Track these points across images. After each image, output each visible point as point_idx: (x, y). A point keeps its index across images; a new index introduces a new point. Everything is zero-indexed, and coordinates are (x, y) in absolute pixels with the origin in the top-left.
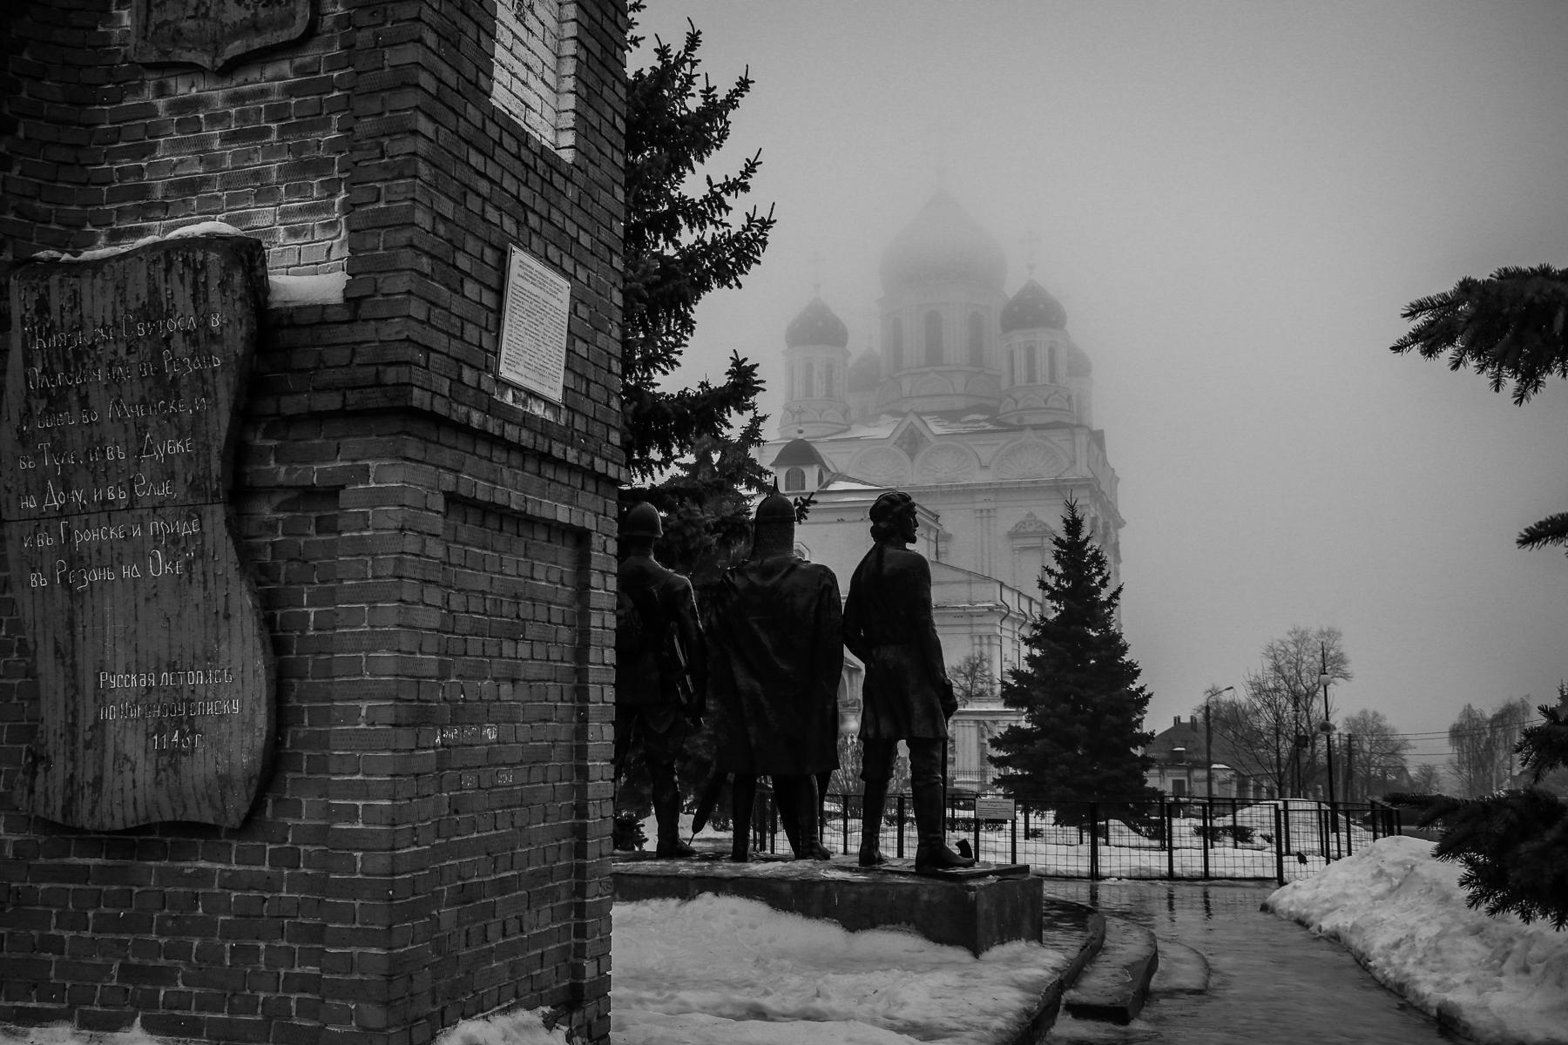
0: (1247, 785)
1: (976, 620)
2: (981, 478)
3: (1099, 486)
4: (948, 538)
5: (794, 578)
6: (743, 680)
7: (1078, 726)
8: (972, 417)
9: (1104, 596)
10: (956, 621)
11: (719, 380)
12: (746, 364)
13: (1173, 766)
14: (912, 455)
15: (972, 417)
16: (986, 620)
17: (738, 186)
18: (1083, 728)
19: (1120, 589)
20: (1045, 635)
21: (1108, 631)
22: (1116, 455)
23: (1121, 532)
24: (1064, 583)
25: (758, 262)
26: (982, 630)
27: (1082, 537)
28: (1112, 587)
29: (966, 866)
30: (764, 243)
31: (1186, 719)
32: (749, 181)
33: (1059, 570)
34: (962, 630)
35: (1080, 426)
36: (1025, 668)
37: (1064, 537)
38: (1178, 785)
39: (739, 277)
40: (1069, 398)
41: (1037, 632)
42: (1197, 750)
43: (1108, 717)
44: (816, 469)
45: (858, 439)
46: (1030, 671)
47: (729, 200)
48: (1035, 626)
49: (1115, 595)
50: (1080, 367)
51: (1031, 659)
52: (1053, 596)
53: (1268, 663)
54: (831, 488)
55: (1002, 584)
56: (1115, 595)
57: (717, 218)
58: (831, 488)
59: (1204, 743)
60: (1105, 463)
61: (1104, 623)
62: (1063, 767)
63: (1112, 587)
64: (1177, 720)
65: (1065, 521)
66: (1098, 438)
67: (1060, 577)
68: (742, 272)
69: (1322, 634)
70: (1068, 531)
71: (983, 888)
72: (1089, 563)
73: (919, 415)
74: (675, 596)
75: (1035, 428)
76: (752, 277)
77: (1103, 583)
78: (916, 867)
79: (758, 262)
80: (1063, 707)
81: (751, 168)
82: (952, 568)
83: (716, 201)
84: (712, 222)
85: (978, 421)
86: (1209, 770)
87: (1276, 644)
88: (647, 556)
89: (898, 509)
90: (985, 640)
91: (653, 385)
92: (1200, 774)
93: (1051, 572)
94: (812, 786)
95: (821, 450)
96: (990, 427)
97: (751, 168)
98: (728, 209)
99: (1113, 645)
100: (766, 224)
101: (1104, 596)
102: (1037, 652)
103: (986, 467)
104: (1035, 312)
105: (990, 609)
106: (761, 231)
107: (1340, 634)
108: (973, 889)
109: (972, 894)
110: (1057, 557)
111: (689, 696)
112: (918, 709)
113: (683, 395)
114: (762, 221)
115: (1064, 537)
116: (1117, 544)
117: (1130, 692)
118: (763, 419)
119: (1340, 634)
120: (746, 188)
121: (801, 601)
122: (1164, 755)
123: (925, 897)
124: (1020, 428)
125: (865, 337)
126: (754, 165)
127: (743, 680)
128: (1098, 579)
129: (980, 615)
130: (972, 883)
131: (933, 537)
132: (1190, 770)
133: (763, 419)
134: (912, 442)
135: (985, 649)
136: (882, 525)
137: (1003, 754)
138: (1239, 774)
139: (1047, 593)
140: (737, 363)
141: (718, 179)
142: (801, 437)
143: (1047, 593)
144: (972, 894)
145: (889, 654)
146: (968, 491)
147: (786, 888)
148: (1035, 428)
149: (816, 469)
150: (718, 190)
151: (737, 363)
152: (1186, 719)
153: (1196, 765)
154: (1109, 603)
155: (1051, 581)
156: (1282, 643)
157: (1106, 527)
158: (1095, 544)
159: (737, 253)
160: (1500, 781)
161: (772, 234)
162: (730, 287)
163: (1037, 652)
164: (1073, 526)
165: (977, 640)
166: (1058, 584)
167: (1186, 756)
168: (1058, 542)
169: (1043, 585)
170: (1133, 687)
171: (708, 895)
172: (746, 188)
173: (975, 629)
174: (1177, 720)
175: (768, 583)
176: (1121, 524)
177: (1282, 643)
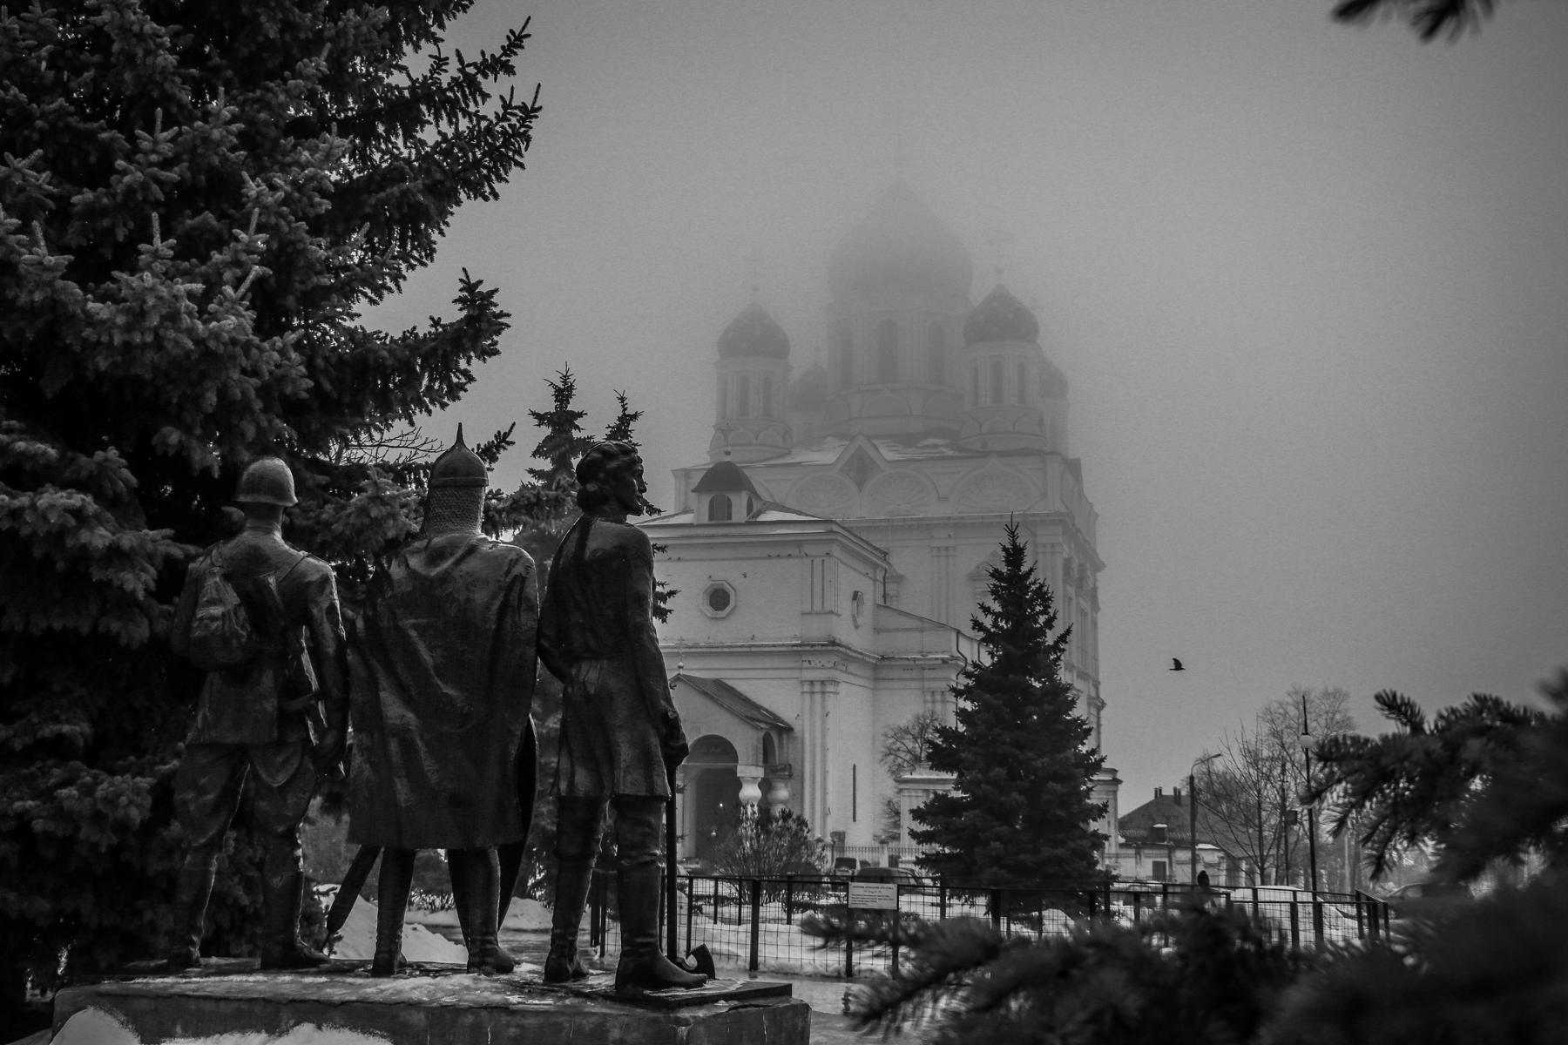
0: (1238, 869)
1: (928, 674)
2: (937, 511)
3: (1074, 525)
4: (899, 579)
5: (472, 564)
6: (394, 710)
7: (1015, 795)
8: (931, 441)
9: (1050, 638)
10: (907, 675)
11: (453, 314)
12: (483, 289)
13: (1153, 846)
14: (860, 484)
15: (931, 441)
16: (939, 674)
17: (498, 65)
18: (1021, 798)
19: (1068, 631)
20: (981, 684)
21: (1051, 679)
22: (1095, 488)
23: (1099, 575)
24: (1003, 624)
25: (522, 166)
26: (934, 685)
27: (1024, 569)
28: (1059, 628)
29: (688, 986)
30: (528, 139)
31: (1168, 791)
32: (513, 61)
33: (997, 607)
34: (914, 684)
35: (1051, 453)
36: (952, 722)
37: (1004, 569)
38: (1159, 869)
39: (496, 185)
40: (1041, 423)
41: (971, 682)
42: (1181, 827)
43: (1051, 784)
44: (744, 497)
45: (799, 464)
46: (962, 728)
47: (487, 84)
48: (969, 675)
49: (1063, 638)
50: (1055, 385)
51: (962, 715)
52: (989, 638)
53: (1265, 728)
54: (762, 518)
55: (958, 632)
56: (1063, 638)
57: (472, 109)
58: (762, 518)
59: (1188, 817)
60: (1081, 495)
61: (1049, 671)
62: (997, 844)
63: (1059, 628)
64: (1158, 792)
65: (1005, 549)
66: (1073, 468)
67: (997, 615)
68: (500, 179)
69: (1326, 695)
70: (1008, 562)
71: (703, 1021)
72: (1032, 599)
73: (869, 438)
74: (301, 593)
75: (1002, 454)
76: (514, 185)
77: (1049, 624)
78: (620, 983)
79: (522, 166)
80: (998, 772)
81: (516, 42)
82: (902, 613)
83: (469, 84)
84: (466, 113)
85: (935, 446)
86: (1193, 851)
87: (1275, 706)
88: (270, 532)
89: (613, 465)
90: (938, 697)
91: (352, 316)
92: (1183, 855)
93: (986, 610)
94: (490, 870)
95: (757, 478)
96: (950, 453)
97: (516, 42)
98: (485, 96)
99: (1059, 697)
100: (529, 113)
101: (1050, 638)
102: (969, 706)
103: (945, 499)
104: (1006, 322)
105: (944, 661)
106: (522, 121)
107: (1347, 695)
108: (686, 1022)
109: (683, 1031)
110: (994, 592)
111: (321, 734)
112: (626, 753)
113: (410, 335)
114: (523, 108)
115: (1004, 569)
116: (1095, 589)
117: (1078, 755)
118: (635, 417)
119: (1347, 695)
120: (510, 70)
121: (480, 597)
122: (1142, 833)
123: (615, 1034)
124: (985, 455)
125: (809, 350)
126: (520, 38)
127: (394, 710)
128: (1042, 619)
129: (932, 668)
130: (685, 1014)
131: (880, 576)
132: (1171, 850)
133: (635, 417)
134: (860, 469)
135: (939, 707)
136: (591, 487)
137: (926, 828)
138: (1229, 856)
139: (982, 635)
140: (469, 287)
141: (472, 56)
142: (728, 459)
143: (982, 635)
144: (683, 1031)
145: (590, 674)
146: (925, 527)
147: (418, 1018)
148: (1002, 454)
149: (744, 497)
150: (471, 70)
151: (469, 287)
152: (1168, 791)
153: (1180, 844)
154: (1055, 647)
155: (988, 621)
156: (1281, 704)
157: (1082, 569)
158: (1039, 575)
159: (492, 152)
160: (821, 858)
161: (537, 127)
162: (486, 199)
163: (969, 706)
164: (1014, 555)
165: (929, 698)
166: (995, 625)
167: (1168, 835)
168: (996, 574)
169: (977, 625)
170: (1083, 749)
171: (307, 1028)
172: (510, 70)
173: (927, 684)
174: (1158, 792)
175: (434, 572)
176: (1099, 567)
177: (1281, 704)
